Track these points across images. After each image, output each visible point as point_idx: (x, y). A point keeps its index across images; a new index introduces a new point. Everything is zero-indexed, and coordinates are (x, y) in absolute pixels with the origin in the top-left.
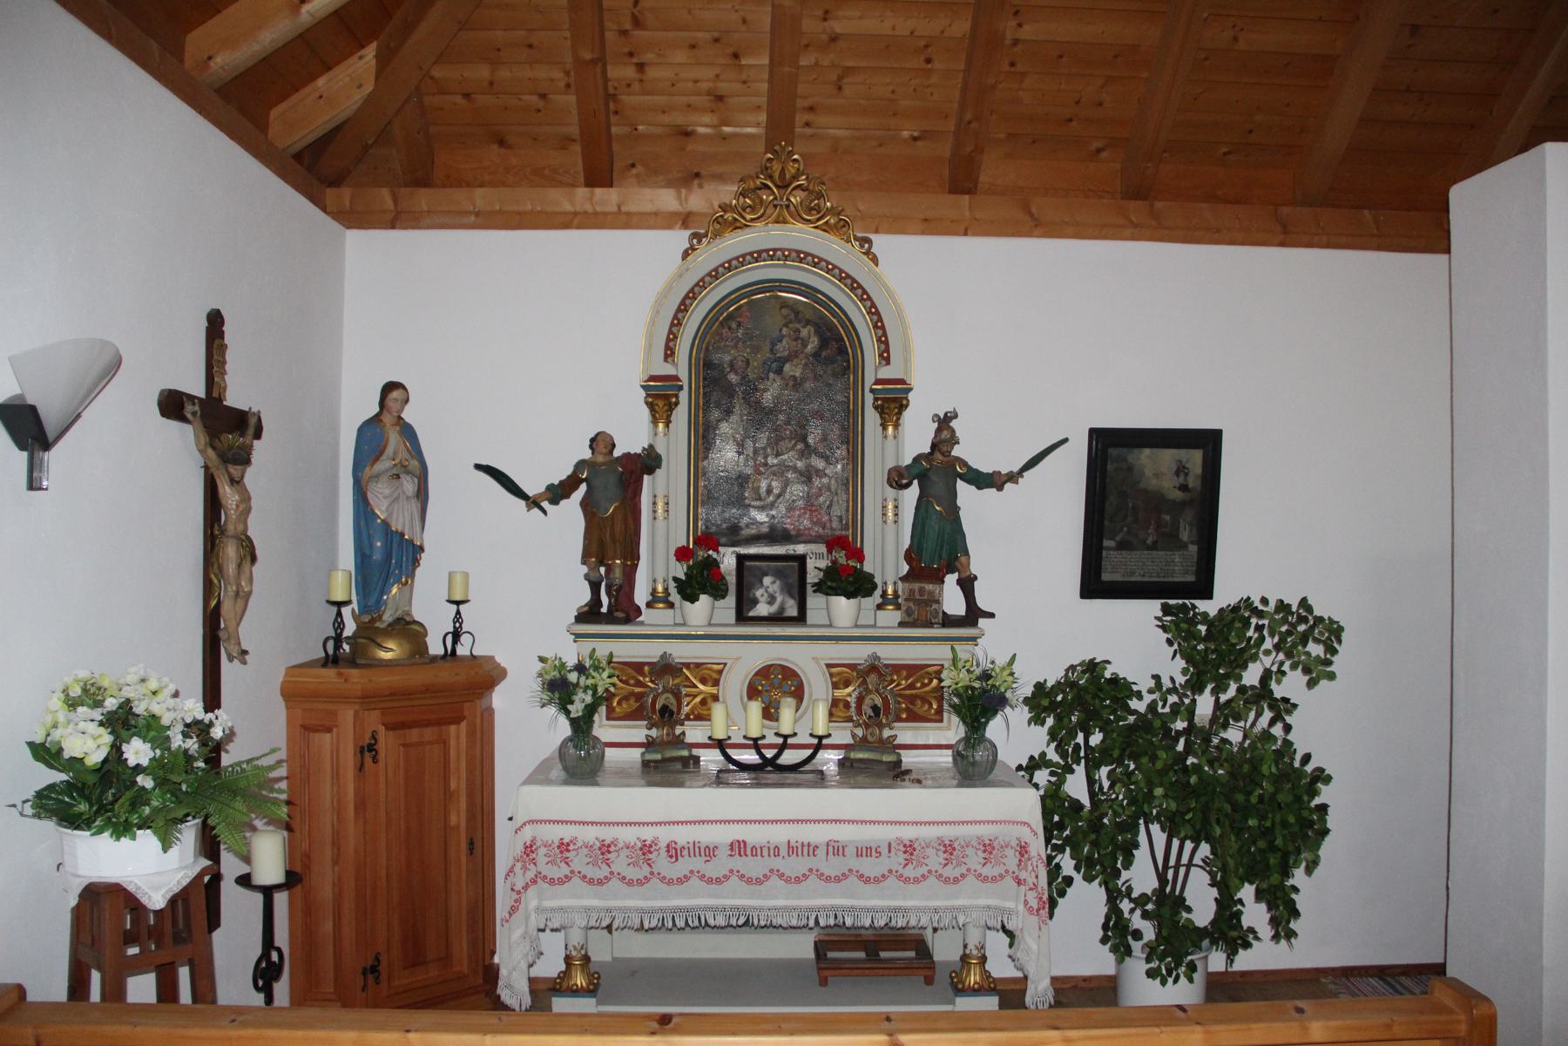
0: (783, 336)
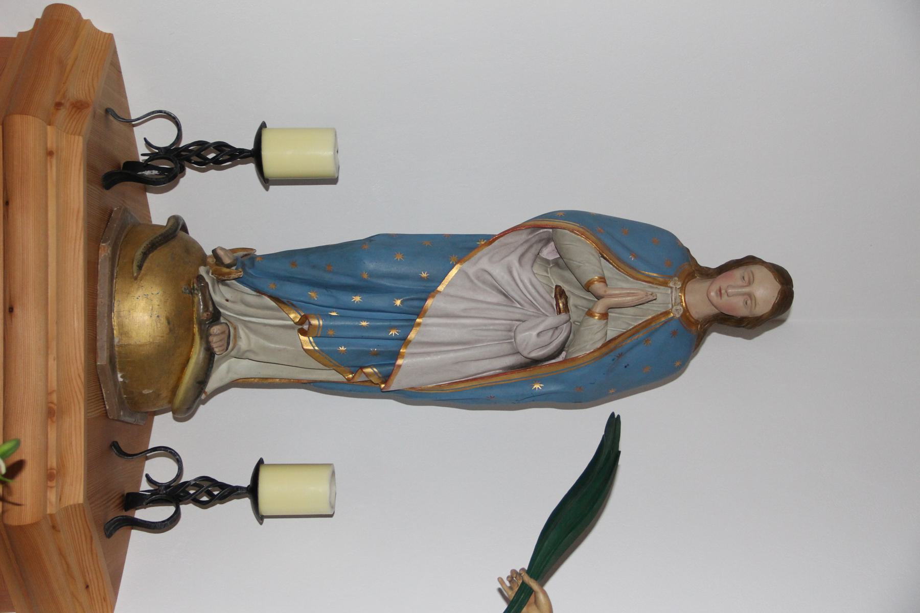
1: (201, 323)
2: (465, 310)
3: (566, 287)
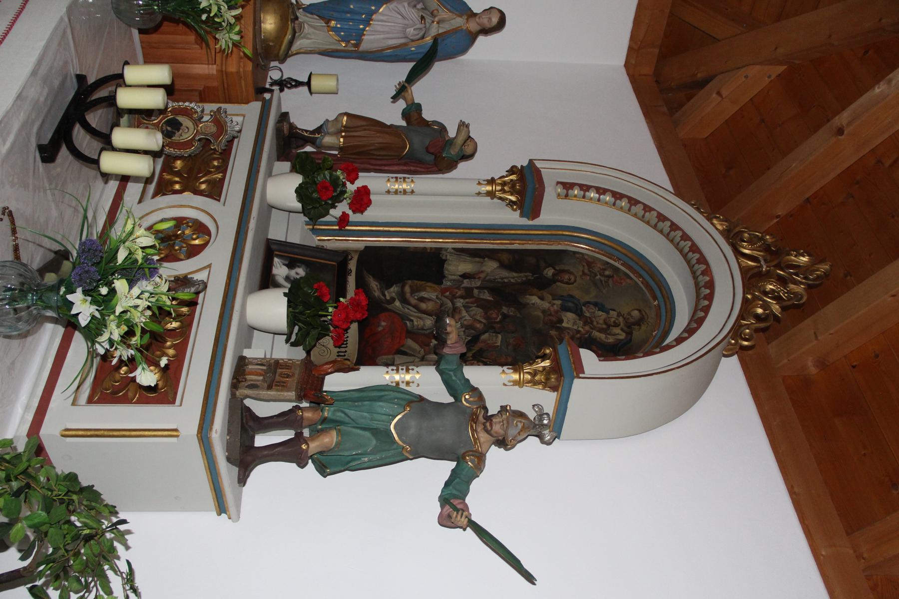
0: (608, 313)
1: (292, 19)
2: (381, 459)
3: (424, 15)
